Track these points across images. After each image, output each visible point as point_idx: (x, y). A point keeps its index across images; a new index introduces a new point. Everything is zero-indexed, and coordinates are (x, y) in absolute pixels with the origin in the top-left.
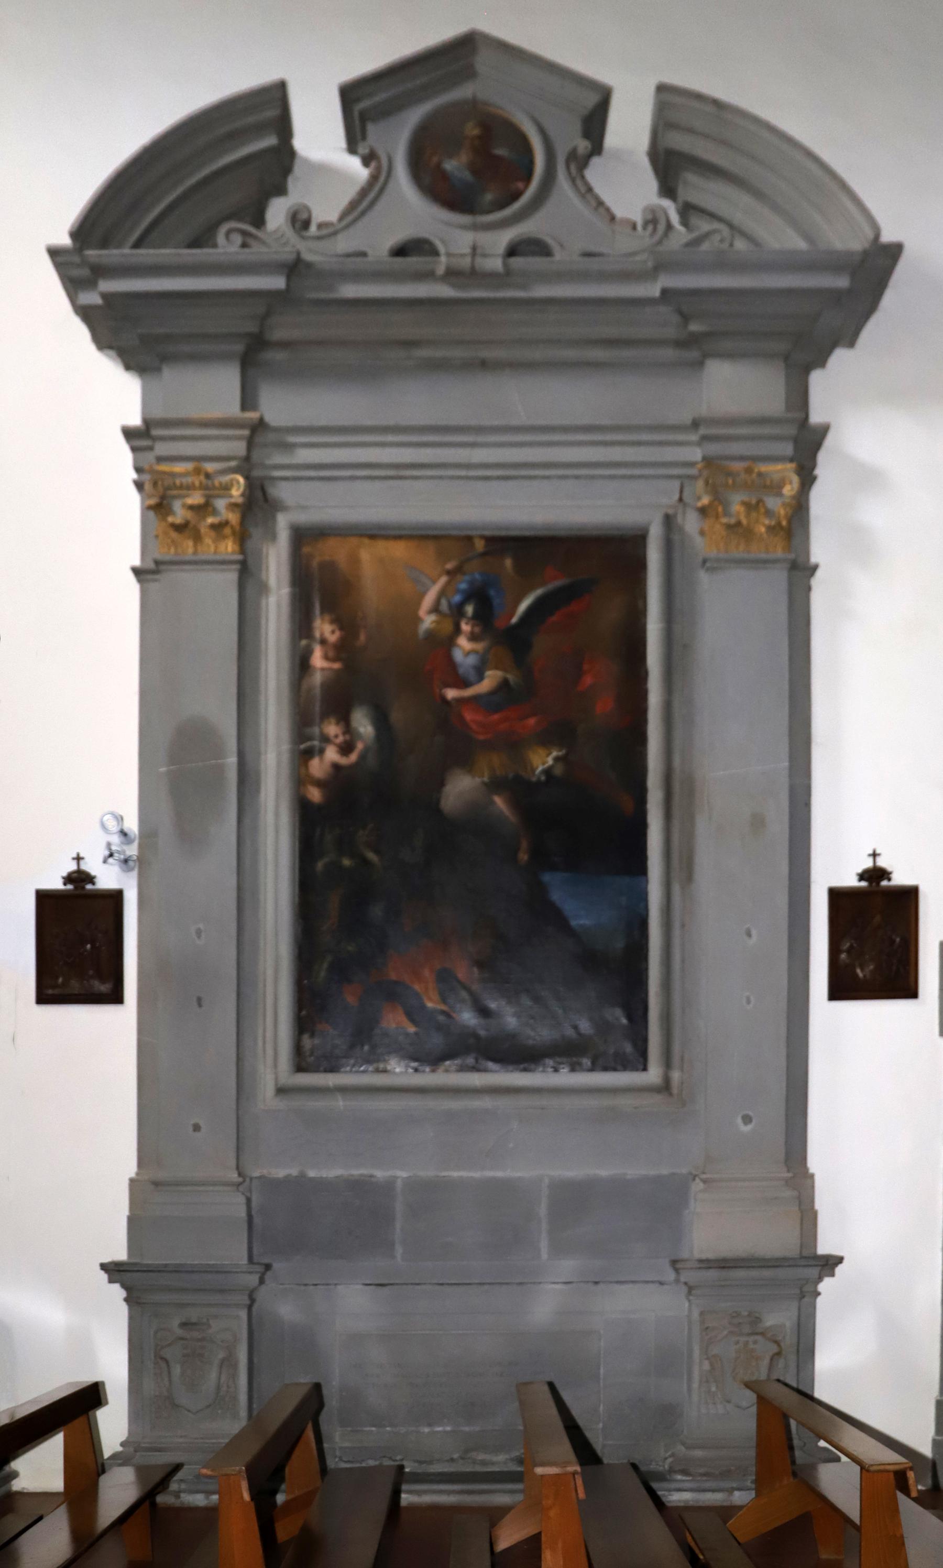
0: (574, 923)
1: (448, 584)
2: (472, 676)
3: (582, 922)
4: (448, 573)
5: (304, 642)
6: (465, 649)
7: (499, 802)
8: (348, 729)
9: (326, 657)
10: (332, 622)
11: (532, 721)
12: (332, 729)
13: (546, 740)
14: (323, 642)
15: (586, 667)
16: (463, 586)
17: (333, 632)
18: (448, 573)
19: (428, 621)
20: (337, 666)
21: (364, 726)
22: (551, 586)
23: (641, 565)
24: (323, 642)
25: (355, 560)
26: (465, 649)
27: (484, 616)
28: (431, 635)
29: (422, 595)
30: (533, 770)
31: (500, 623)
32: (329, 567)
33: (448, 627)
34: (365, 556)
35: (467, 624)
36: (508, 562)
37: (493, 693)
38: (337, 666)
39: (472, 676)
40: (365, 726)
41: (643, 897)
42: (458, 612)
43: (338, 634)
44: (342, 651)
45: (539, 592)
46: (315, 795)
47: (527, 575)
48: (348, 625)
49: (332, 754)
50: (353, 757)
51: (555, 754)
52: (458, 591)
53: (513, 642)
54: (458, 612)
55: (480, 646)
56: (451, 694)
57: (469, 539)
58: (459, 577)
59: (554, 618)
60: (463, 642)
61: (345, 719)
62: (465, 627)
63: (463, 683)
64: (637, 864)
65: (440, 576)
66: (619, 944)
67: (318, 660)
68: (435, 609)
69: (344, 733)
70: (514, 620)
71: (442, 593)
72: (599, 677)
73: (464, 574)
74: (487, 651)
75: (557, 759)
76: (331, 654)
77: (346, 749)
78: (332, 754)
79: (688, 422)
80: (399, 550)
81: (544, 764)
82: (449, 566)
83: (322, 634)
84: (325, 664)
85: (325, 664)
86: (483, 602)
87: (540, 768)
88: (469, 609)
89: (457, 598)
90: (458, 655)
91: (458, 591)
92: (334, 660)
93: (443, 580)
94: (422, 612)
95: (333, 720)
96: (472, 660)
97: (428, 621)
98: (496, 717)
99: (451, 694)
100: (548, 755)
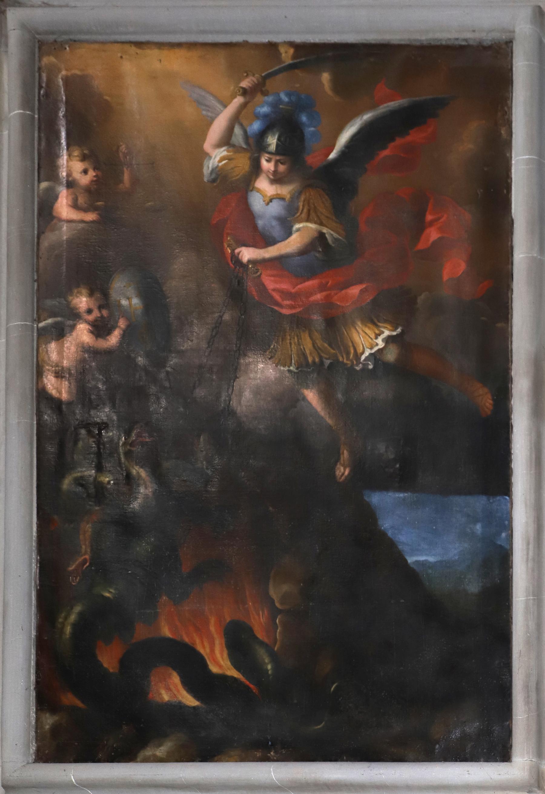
0: (411, 560)
1: (244, 106)
2: (276, 231)
3: (422, 558)
4: (244, 92)
5: (44, 185)
6: (267, 196)
7: (311, 396)
8: (104, 299)
9: (75, 206)
10: (84, 158)
11: (355, 291)
12: (82, 301)
13: (372, 317)
14: (71, 184)
15: (429, 217)
16: (265, 109)
17: (85, 172)
18: (244, 92)
19: (216, 157)
20: (90, 217)
21: (127, 297)
22: (383, 109)
23: (503, 80)
24: (71, 184)
25: (116, 77)
26: (267, 196)
27: (293, 149)
28: (220, 176)
29: (210, 122)
30: (357, 356)
31: (313, 160)
32: (78, 86)
33: (243, 164)
34: (128, 67)
35: (268, 161)
36: (326, 77)
37: (303, 252)
38: (90, 217)
39: (276, 231)
40: (129, 299)
41: (506, 524)
42: (257, 145)
43: (92, 173)
44: (100, 195)
45: (367, 117)
46: (58, 388)
47: (351, 93)
48: (106, 162)
49: (82, 333)
50: (114, 339)
51: (387, 333)
52: (257, 116)
53: (330, 185)
54: (257, 145)
55: (286, 190)
56: (247, 254)
57: (272, 46)
58: (259, 98)
59: (385, 153)
60: (263, 184)
61: (100, 290)
62: (267, 165)
63: (265, 240)
64: (498, 482)
65: (233, 97)
66: (473, 587)
67: (63, 208)
68: (226, 140)
69: (100, 308)
70: (332, 156)
71: (235, 119)
72: (450, 228)
73: (265, 93)
74: (295, 197)
75: (389, 340)
76: (81, 201)
77: (100, 329)
78: (82, 333)
79: (273, 201)
80: (176, 63)
81: (371, 348)
82: (245, 84)
83: (69, 175)
84: (74, 215)
85: (74, 215)
86: (290, 131)
87: (367, 353)
88: (272, 141)
89: (256, 126)
90: (257, 203)
91: (257, 116)
92: (85, 210)
93: (238, 100)
94: (207, 146)
95: (84, 291)
96: (276, 209)
97: (216, 157)
98: (309, 283)
99: (247, 254)
100: (377, 336)
